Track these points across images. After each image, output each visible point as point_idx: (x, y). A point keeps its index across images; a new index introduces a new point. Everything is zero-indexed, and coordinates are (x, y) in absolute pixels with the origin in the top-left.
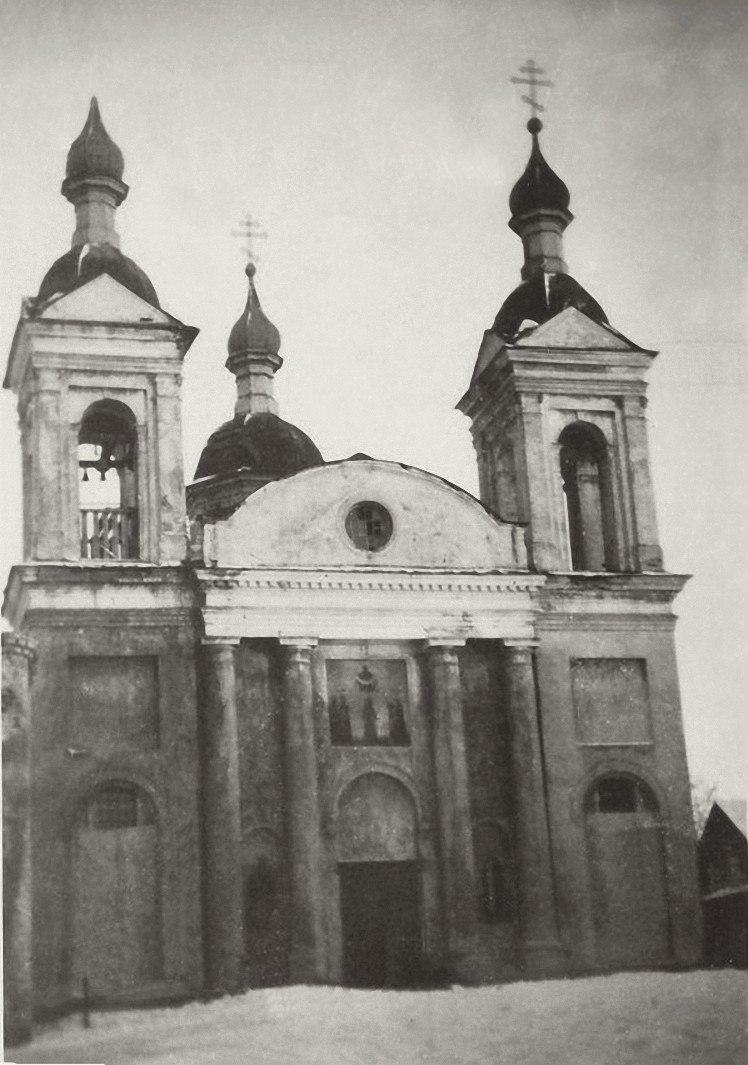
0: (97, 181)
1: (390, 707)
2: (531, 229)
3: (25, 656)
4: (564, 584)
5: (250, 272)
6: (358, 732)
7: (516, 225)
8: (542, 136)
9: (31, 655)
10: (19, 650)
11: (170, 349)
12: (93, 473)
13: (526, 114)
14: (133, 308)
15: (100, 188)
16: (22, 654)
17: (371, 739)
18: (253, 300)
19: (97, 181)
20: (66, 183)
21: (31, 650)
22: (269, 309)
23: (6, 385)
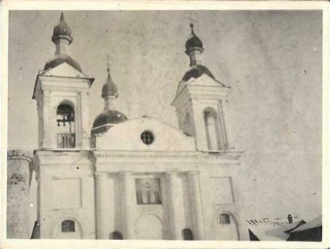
0: (64, 36)
1: (155, 193)
2: (191, 53)
3: (28, 161)
4: (207, 154)
5: (108, 70)
6: (145, 200)
7: (188, 52)
8: (194, 28)
9: (30, 160)
10: (24, 158)
11: (86, 85)
12: (61, 123)
13: (107, 67)
14: (74, 73)
15: (63, 38)
16: (26, 160)
17: (149, 203)
18: (109, 76)
19: (64, 36)
20: (53, 37)
21: (30, 158)
22: (198, 35)
23: (33, 98)
